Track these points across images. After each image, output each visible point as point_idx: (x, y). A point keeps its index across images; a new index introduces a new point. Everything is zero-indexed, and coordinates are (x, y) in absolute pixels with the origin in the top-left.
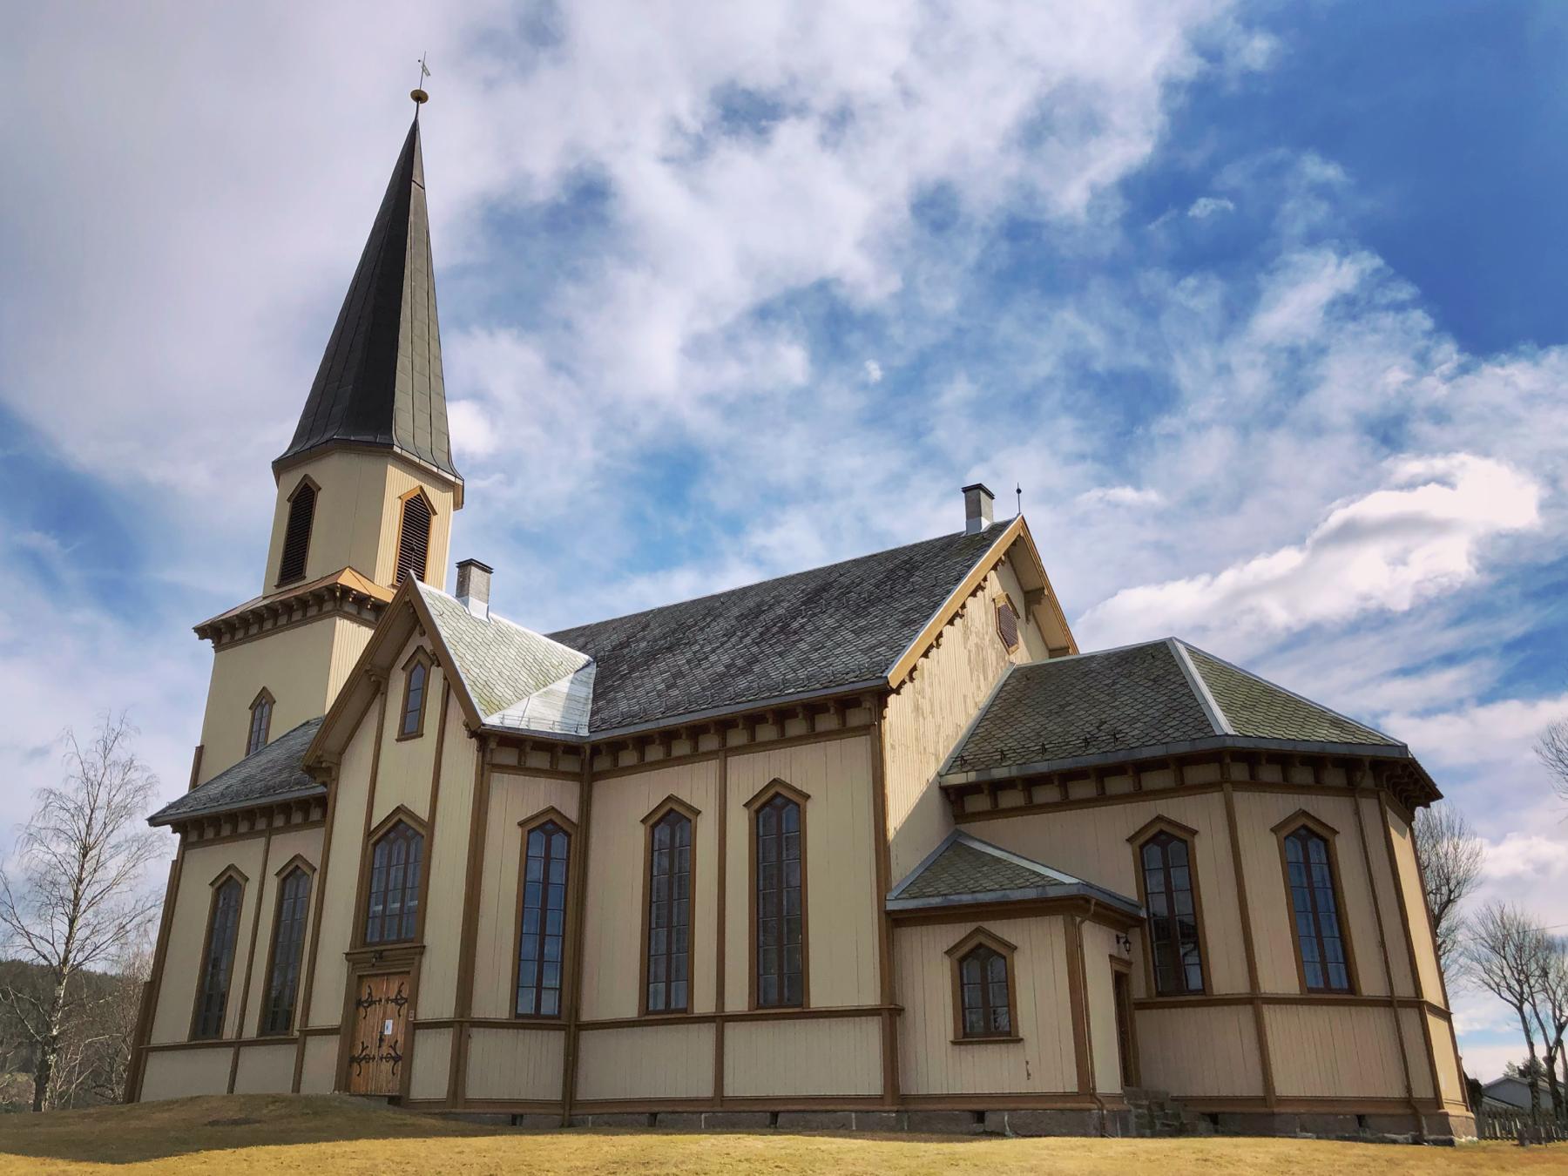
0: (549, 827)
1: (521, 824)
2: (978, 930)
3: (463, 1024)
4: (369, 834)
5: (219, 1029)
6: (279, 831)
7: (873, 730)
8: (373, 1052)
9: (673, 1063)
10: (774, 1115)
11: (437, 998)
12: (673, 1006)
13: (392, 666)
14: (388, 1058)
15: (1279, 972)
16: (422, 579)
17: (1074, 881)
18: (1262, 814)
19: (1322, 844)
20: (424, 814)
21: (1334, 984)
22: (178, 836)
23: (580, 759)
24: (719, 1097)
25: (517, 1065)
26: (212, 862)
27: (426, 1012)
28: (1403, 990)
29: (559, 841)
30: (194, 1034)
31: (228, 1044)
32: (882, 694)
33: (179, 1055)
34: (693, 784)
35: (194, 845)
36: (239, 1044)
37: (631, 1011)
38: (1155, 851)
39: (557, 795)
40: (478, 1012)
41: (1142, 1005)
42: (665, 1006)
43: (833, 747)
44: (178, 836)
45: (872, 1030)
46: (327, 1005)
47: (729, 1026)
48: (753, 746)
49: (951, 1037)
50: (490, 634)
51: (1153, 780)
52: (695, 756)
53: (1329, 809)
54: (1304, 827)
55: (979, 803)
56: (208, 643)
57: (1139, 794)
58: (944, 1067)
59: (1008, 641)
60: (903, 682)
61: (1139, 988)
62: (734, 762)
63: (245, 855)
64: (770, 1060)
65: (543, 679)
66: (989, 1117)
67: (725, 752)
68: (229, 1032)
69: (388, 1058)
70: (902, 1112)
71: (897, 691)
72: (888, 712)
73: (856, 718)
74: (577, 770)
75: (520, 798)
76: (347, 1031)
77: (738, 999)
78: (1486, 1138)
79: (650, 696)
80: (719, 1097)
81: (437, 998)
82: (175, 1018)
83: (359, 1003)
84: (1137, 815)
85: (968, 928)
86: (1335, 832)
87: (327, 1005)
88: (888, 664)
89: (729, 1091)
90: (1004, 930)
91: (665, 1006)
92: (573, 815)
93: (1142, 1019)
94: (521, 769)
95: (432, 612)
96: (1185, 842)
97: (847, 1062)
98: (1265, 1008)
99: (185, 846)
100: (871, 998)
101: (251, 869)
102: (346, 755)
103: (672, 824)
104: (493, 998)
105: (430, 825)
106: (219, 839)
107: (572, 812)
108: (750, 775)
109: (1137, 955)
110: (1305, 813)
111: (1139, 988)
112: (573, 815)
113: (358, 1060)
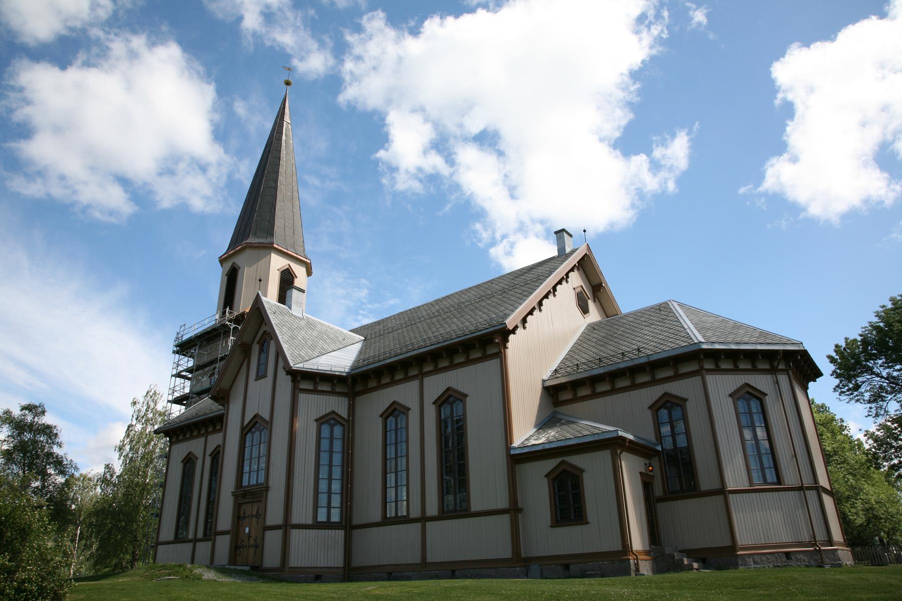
0: (332, 422)
2: (563, 462)
3: (287, 526)
4: (243, 429)
7: (500, 355)
10: (454, 570)
12: (391, 513)
13: (253, 342)
16: (266, 296)
17: (631, 437)
18: (721, 386)
19: (758, 402)
20: (267, 417)
21: (769, 480)
23: (355, 383)
26: (181, 450)
27: (270, 522)
28: (807, 481)
31: (190, 541)
32: (505, 333)
33: (171, 546)
34: (405, 393)
36: (195, 540)
38: (664, 413)
39: (339, 405)
40: (295, 520)
41: (660, 500)
42: (178, 539)
43: (480, 366)
45: (506, 519)
46: (225, 520)
47: (428, 524)
48: (437, 371)
49: (549, 523)
50: (303, 323)
51: (662, 374)
52: (407, 379)
53: (762, 382)
54: (748, 393)
55: (565, 396)
57: (654, 382)
58: (547, 538)
59: (585, 310)
60: (516, 327)
61: (658, 491)
62: (427, 380)
63: (195, 446)
64: (450, 539)
65: (344, 345)
66: (572, 567)
70: (520, 564)
71: (513, 331)
72: (509, 345)
73: (492, 350)
74: (346, 391)
75: (314, 406)
76: (235, 532)
79: (392, 349)
80: (424, 563)
81: (274, 516)
84: (654, 393)
86: (765, 395)
87: (225, 520)
88: (506, 316)
89: (430, 559)
90: (576, 460)
92: (345, 415)
93: (660, 506)
95: (268, 311)
96: (681, 406)
97: (488, 538)
98: (730, 496)
99: (172, 443)
100: (504, 504)
101: (199, 453)
102: (232, 392)
106: (185, 439)
107: (343, 412)
108: (436, 385)
109: (657, 473)
110: (747, 385)
111: (658, 491)
112: (345, 415)
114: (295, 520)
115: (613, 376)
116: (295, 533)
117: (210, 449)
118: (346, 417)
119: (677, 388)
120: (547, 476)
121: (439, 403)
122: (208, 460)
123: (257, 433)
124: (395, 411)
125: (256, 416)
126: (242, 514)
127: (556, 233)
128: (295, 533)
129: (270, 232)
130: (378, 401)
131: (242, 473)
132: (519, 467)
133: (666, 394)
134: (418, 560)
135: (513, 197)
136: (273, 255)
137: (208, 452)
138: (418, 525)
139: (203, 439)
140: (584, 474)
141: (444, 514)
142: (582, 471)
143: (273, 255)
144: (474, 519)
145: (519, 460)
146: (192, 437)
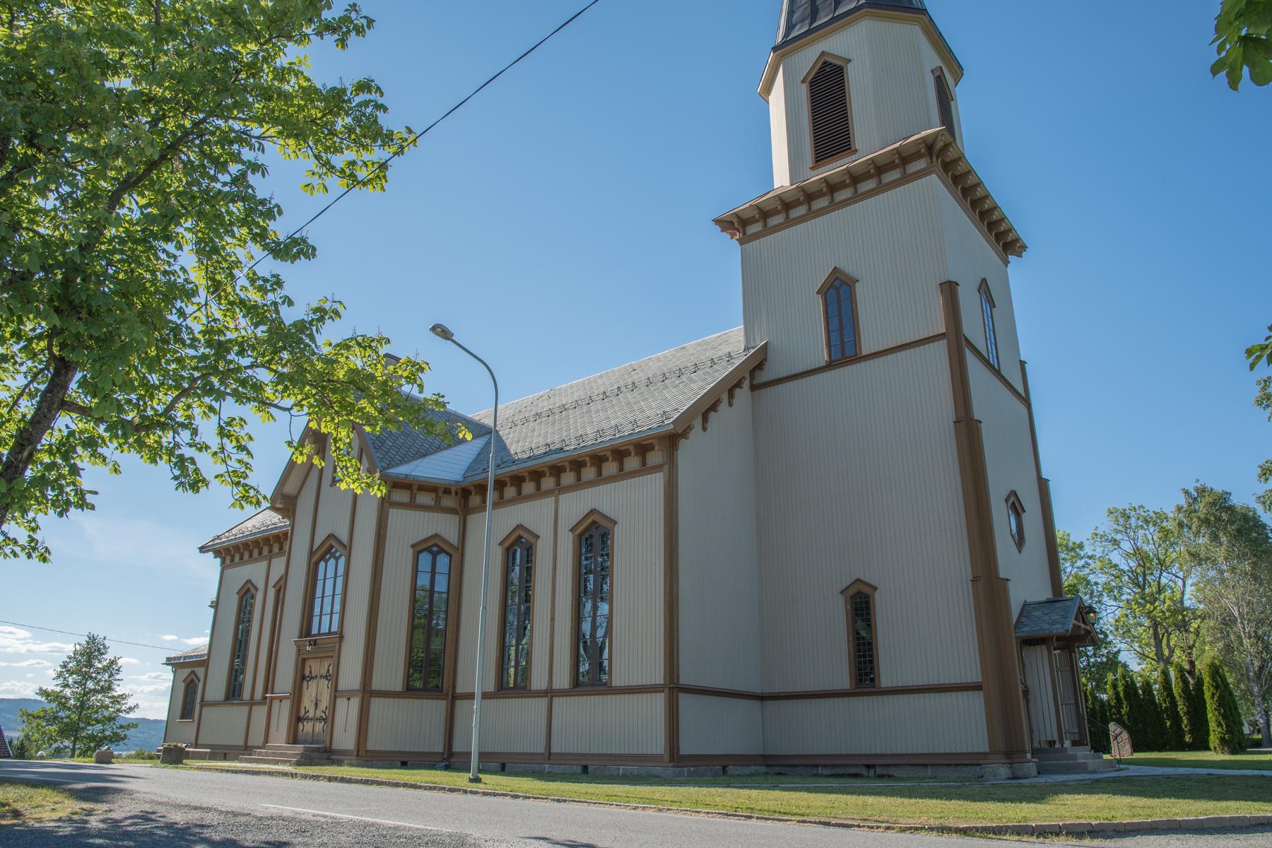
1: (413, 546)
4: (311, 553)
5: (240, 694)
8: (311, 715)
9: (520, 722)
11: (350, 676)
22: (218, 560)
24: (549, 755)
25: (417, 720)
29: (443, 560)
30: (227, 698)
34: (533, 514)
35: (229, 567)
36: (252, 703)
37: (399, 687)
39: (446, 526)
40: (377, 684)
42: (511, 683)
44: (218, 560)
52: (539, 493)
63: (254, 571)
64: (583, 723)
67: (559, 489)
68: (246, 694)
77: (563, 679)
80: (549, 755)
82: (216, 686)
83: (303, 678)
89: (555, 749)
91: (511, 683)
94: (412, 505)
103: (519, 549)
104: (390, 673)
108: (575, 505)
114: (377, 684)
116: (377, 705)
117: (274, 579)
118: (456, 544)
121: (507, 544)
122: (271, 593)
123: (332, 561)
125: (331, 536)
126: (307, 673)
128: (377, 705)
130: (491, 527)
134: (540, 748)
135: (984, 281)
137: (271, 583)
138: (543, 702)
139: (265, 563)
141: (578, 686)
146: (252, 559)
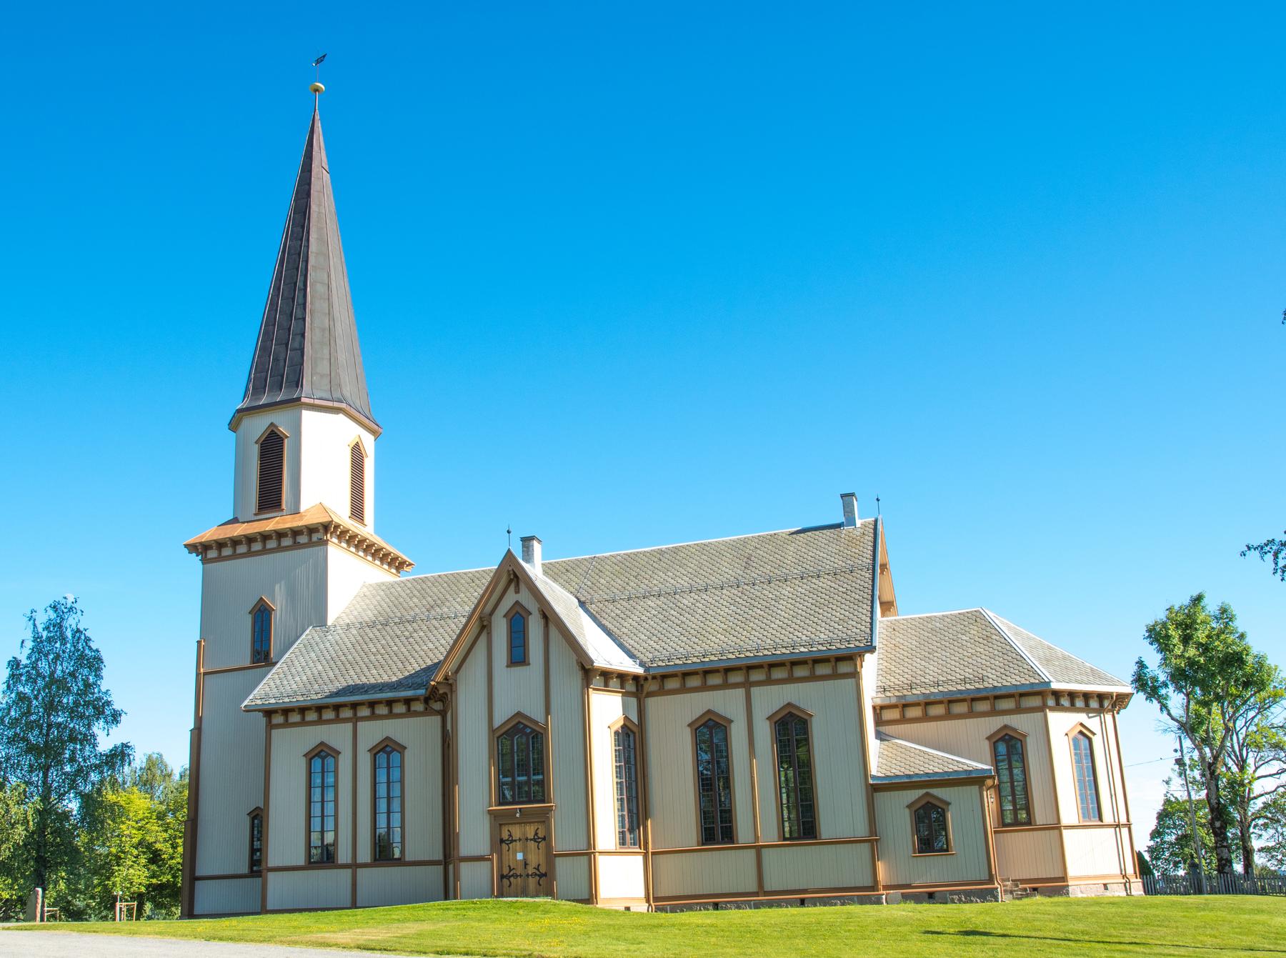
1: (988, 738)
2: (927, 794)
4: (492, 731)
6: (278, 726)
14: (534, 875)
15: (768, 831)
40: (359, 860)
54: (1081, 732)
56: (195, 560)
57: (994, 712)
69: (534, 875)
78: (1156, 893)
84: (995, 723)
85: (921, 792)
105: (546, 729)
113: (508, 877)
115: (950, 701)
119: (1020, 722)
120: (909, 807)
124: (387, 749)
127: (842, 496)
129: (298, 383)
131: (310, 832)
132: (877, 795)
133: (1006, 727)
136: (304, 412)
140: (733, 725)
142: (730, 721)
143: (304, 412)
144: (693, 695)
145: (876, 789)
